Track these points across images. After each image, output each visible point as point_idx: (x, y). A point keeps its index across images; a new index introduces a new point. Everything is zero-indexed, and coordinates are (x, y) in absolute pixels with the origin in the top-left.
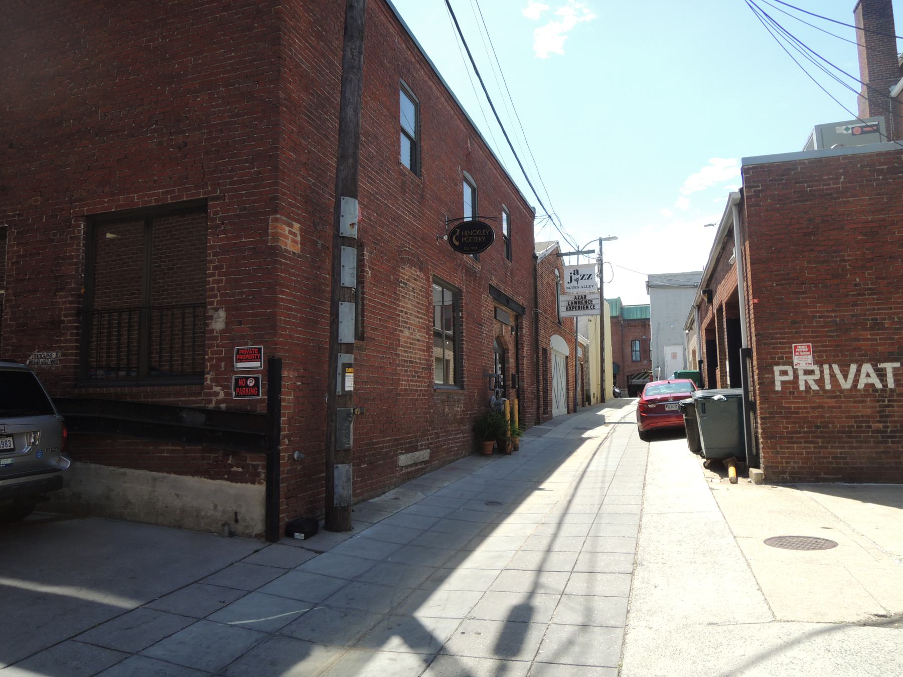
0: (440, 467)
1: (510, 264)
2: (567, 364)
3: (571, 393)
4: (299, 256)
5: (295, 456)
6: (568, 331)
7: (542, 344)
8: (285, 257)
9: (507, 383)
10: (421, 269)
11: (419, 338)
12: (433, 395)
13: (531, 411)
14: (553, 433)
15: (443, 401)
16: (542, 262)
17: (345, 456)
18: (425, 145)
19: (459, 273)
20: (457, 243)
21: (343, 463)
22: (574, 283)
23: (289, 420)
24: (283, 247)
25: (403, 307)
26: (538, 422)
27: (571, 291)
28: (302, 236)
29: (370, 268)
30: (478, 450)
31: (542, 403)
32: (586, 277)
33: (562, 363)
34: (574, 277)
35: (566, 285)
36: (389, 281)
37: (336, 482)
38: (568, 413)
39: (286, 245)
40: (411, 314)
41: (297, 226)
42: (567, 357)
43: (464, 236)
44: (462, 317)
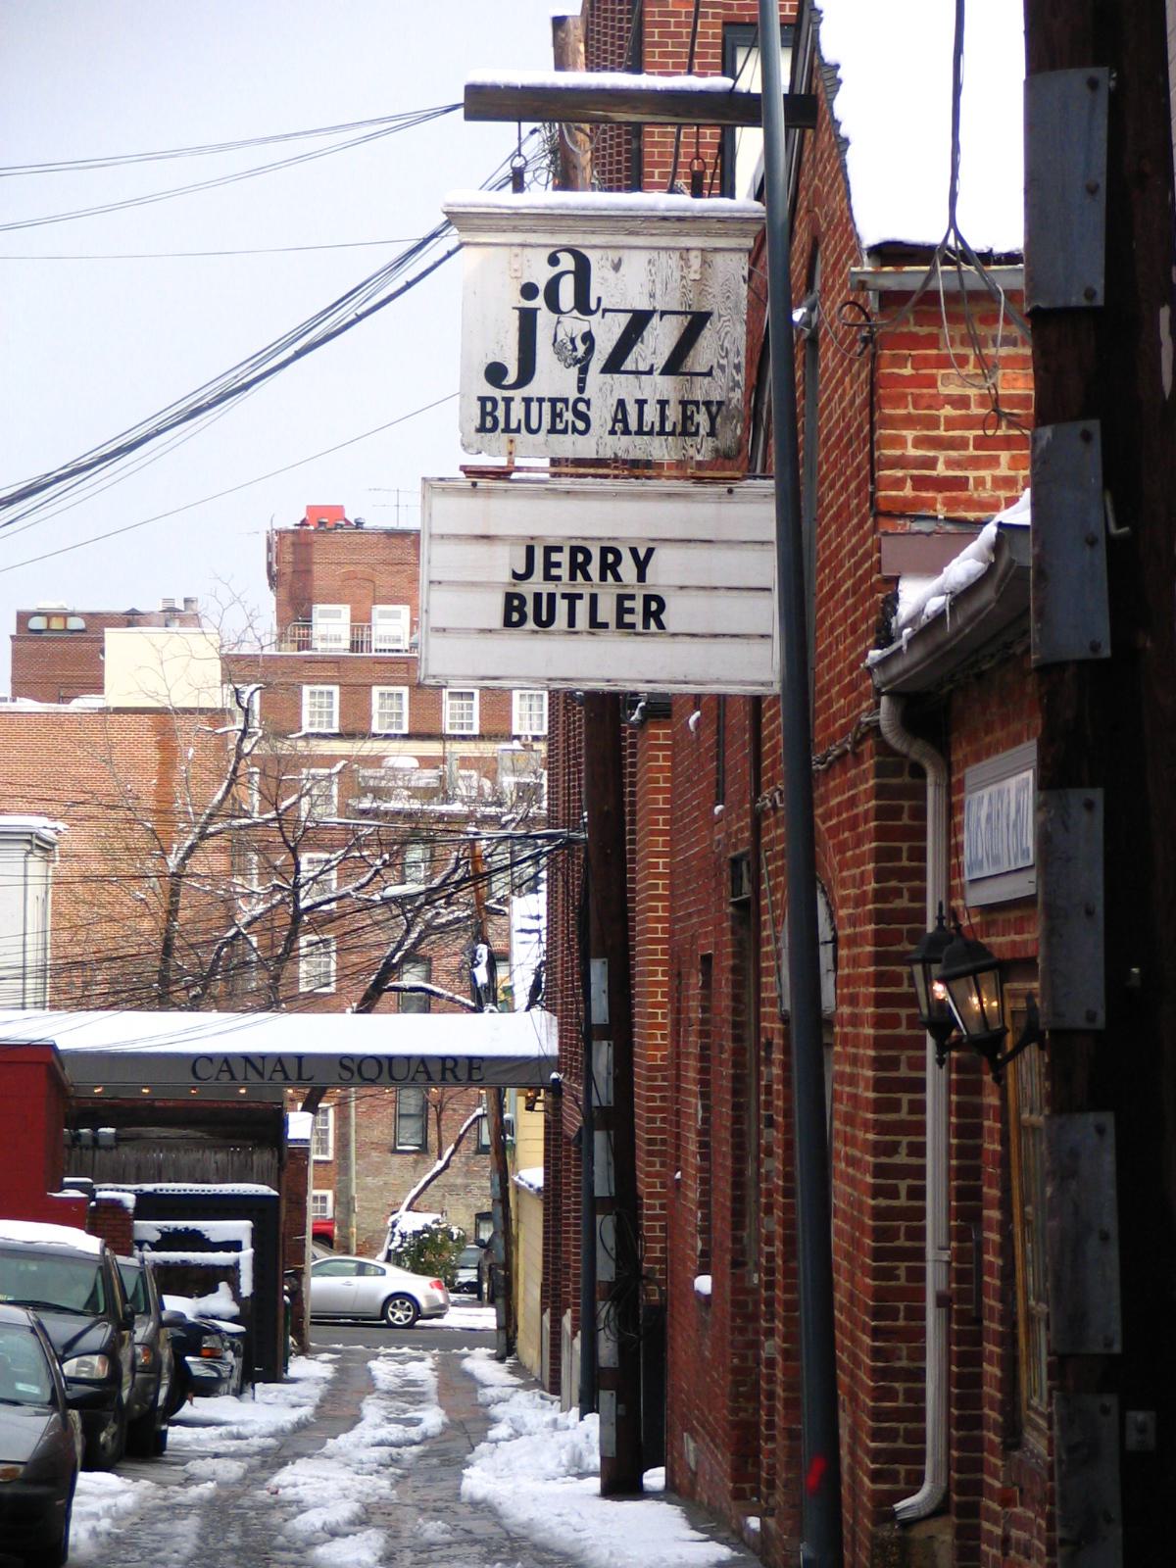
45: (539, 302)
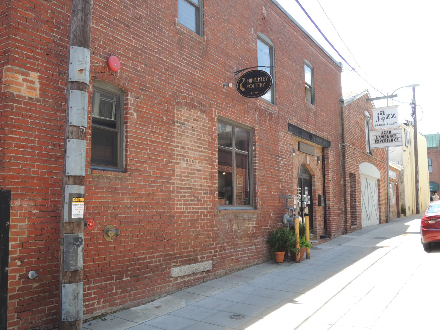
0: (226, 274)
1: (313, 107)
2: (379, 185)
3: (383, 208)
4: (38, 100)
5: (30, 276)
6: (381, 160)
7: (349, 169)
8: (19, 102)
9: (314, 202)
10: (202, 111)
11: (200, 168)
12: (218, 216)
13: (337, 223)
14: (353, 241)
15: (230, 220)
16: (350, 105)
17: (74, 277)
18: (208, 10)
19: (251, 115)
20: (243, 90)
21: (70, 282)
22: (381, 122)
23: (22, 245)
24: (15, 93)
25: (178, 142)
26: (345, 232)
27: (380, 127)
28: (41, 84)
29: (135, 110)
30: (272, 259)
31: (349, 216)
32: (390, 116)
33: (374, 185)
34: (381, 117)
35: (375, 123)
36: (162, 122)
37: (64, 300)
38: (380, 223)
39: (20, 91)
40: (190, 149)
41: (34, 76)
42: (379, 180)
43: (249, 84)
44: (255, 151)
45: (379, 115)
